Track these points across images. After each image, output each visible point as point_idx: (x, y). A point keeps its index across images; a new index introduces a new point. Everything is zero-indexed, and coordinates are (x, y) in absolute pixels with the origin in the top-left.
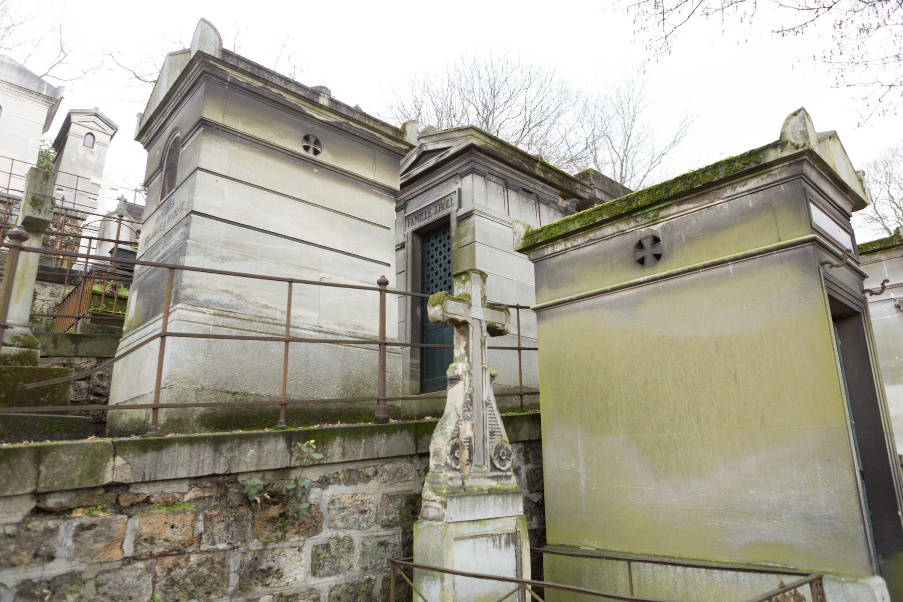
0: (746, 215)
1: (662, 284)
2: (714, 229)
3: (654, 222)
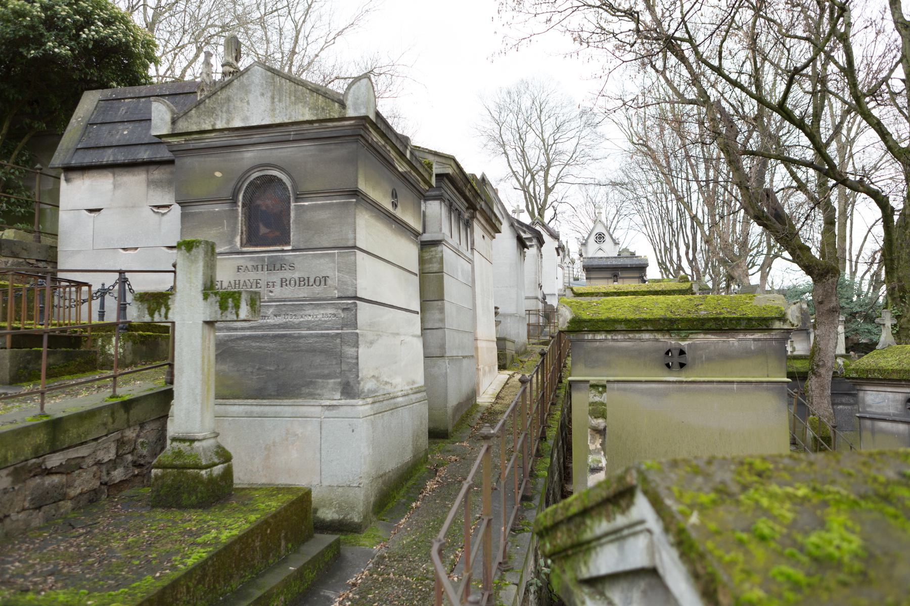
0: (746, 354)
1: (684, 385)
2: (726, 357)
3: (684, 339)
